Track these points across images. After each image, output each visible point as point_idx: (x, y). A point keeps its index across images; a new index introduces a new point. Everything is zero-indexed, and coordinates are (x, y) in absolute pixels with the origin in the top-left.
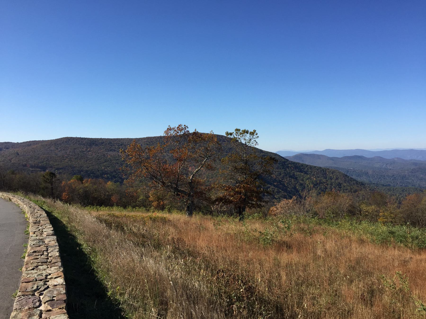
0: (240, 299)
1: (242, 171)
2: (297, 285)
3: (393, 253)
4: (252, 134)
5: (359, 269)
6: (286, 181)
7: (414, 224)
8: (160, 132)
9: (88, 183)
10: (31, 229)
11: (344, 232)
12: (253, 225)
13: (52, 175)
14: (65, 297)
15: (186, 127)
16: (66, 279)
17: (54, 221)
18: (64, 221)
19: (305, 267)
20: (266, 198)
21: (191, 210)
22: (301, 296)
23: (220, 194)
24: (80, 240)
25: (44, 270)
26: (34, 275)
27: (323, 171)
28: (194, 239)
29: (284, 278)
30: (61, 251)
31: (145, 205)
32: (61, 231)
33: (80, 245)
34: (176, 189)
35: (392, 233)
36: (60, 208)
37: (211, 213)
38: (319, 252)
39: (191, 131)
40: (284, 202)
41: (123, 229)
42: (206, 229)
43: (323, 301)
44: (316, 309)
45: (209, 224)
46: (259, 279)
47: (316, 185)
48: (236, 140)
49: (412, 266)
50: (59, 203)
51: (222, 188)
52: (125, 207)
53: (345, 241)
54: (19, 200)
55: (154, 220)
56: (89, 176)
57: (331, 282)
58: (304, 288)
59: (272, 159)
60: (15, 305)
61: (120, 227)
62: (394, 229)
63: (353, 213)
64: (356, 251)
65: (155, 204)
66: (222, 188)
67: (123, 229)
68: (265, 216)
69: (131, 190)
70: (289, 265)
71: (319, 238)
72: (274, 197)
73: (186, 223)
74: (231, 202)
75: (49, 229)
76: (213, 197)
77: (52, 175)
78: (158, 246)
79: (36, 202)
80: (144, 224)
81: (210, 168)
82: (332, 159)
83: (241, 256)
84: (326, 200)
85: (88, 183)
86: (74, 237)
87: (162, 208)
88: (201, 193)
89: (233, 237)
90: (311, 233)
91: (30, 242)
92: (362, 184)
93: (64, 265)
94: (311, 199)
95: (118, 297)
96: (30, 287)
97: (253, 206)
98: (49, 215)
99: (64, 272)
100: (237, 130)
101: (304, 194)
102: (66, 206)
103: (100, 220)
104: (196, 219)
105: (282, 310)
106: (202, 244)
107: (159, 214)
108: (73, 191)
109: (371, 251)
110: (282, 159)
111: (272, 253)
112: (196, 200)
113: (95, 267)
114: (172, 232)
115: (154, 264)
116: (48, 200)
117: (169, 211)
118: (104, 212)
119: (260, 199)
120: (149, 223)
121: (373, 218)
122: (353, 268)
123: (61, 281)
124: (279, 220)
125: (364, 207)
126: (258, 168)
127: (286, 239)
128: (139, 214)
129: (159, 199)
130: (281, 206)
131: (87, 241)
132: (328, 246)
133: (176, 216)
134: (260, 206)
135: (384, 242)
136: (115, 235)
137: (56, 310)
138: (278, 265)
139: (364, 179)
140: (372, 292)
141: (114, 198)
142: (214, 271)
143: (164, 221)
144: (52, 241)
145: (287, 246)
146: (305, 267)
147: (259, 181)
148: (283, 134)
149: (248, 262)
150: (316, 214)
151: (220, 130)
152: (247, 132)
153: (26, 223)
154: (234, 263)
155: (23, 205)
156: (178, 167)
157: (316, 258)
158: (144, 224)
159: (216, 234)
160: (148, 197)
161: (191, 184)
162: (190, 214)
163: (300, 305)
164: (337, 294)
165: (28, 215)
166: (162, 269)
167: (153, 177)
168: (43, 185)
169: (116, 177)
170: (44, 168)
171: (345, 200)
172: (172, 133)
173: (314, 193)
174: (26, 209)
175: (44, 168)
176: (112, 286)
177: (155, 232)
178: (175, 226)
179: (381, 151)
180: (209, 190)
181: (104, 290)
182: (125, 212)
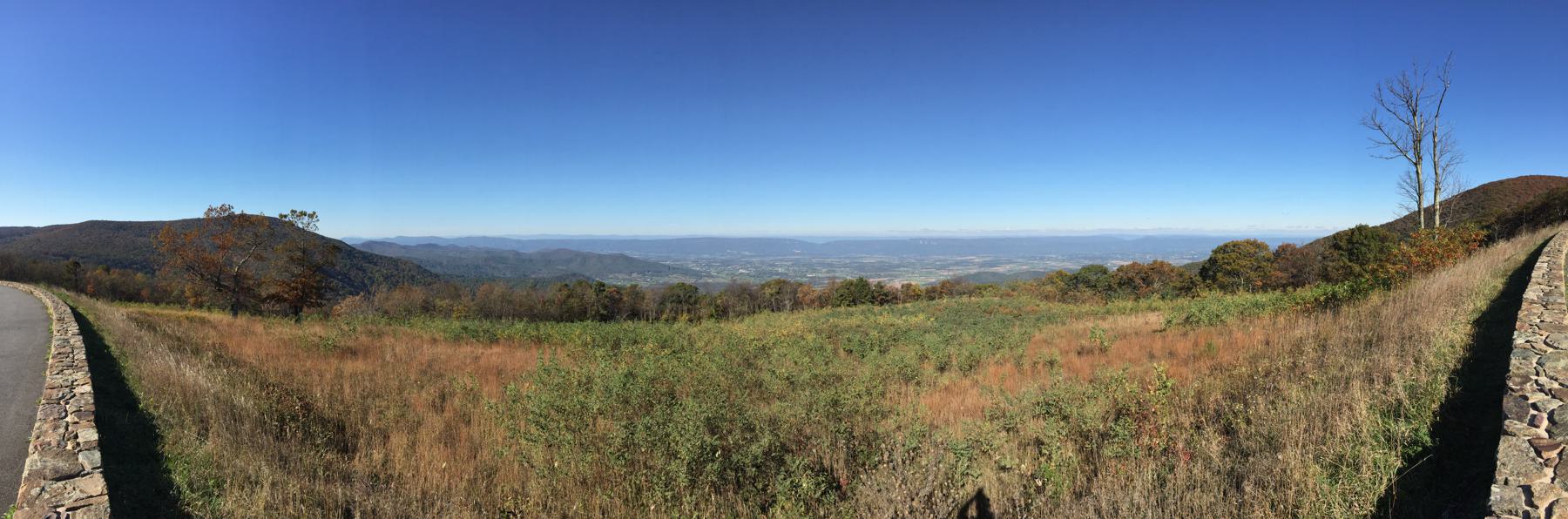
0: (293, 419)
1: (300, 262)
2: (363, 398)
3: (466, 350)
4: (311, 216)
5: (431, 372)
6: (353, 273)
7: (487, 316)
8: (198, 213)
9: (115, 275)
10: (55, 327)
11: (416, 331)
12: (312, 329)
13: (77, 264)
14: (93, 408)
15: (231, 207)
16: (94, 387)
17: (79, 318)
18: (91, 318)
19: (373, 375)
20: (328, 295)
21: (236, 309)
22: (365, 412)
23: (272, 291)
24: (109, 340)
25: (71, 376)
26: (59, 380)
27: (395, 262)
28: (239, 345)
29: (347, 390)
30: (88, 353)
31: (181, 301)
32: (88, 332)
33: (108, 347)
34: (218, 284)
35: (465, 328)
36: (85, 304)
37: (261, 313)
38: (388, 357)
39: (237, 212)
40: (349, 299)
41: (155, 329)
42: (253, 333)
43: (391, 414)
44: (382, 425)
45: (259, 327)
46: (319, 396)
47: (386, 278)
48: (292, 224)
49: (482, 362)
50: (84, 298)
51: (275, 282)
52: (157, 303)
53: (417, 342)
54: (40, 293)
55: (191, 320)
56: (116, 266)
57: (400, 391)
58: (369, 401)
59: (336, 247)
60: (39, 415)
61: (152, 328)
62: (466, 324)
63: (427, 309)
64: (428, 352)
65: (192, 300)
66: (275, 282)
67: (155, 329)
68: (327, 316)
69: (164, 283)
70: (353, 375)
71: (388, 341)
72: (338, 295)
73: (229, 325)
74: (285, 300)
75: (74, 328)
76: (264, 294)
77: (77, 264)
78: (197, 352)
79: (60, 296)
80: (180, 324)
81: (260, 258)
82: (405, 247)
83: (297, 365)
84: (397, 295)
85: (115, 275)
86: (102, 339)
87: (199, 306)
88: (249, 289)
89: (286, 343)
90: (380, 335)
91: (54, 343)
92: (437, 276)
93: (91, 370)
94: (380, 296)
95: (151, 410)
96: (55, 394)
97: (312, 305)
98: (74, 310)
99: (92, 378)
100: (293, 212)
101: (372, 289)
102: (93, 301)
103: (130, 318)
104: (242, 320)
105: (344, 429)
106: (248, 351)
107: (197, 313)
108: (98, 283)
109: (442, 350)
110: (1255, 327)
111: (334, 362)
112: (241, 297)
113: (124, 374)
114: (213, 337)
115: (193, 374)
116: (72, 294)
117: (209, 309)
118: (133, 308)
119: (321, 296)
120: (186, 324)
121: (447, 314)
122: (425, 373)
123: (88, 388)
124: (348, 320)
125: (438, 302)
126: (318, 258)
127: (351, 343)
128: (174, 312)
129: (196, 295)
130: (345, 305)
131: (116, 343)
132: (397, 350)
133: (216, 316)
134: (320, 305)
135: (457, 339)
136: (147, 337)
137: (83, 422)
138: (339, 375)
139: (437, 270)
140: (443, 397)
141: (144, 293)
142: (264, 385)
143: (203, 321)
144: (77, 341)
145: (353, 353)
146: (373, 375)
147: (320, 275)
148: (351, 216)
149: (305, 374)
150: (386, 312)
151: (273, 213)
152: (304, 214)
153: (49, 319)
154: (289, 375)
155: (48, 300)
156: (219, 257)
157: (384, 364)
158: (180, 324)
159: (264, 338)
160: (183, 292)
161: (237, 278)
162: (235, 314)
163: (364, 421)
164: (406, 405)
165: (51, 311)
166: (202, 381)
167: (190, 268)
168: (67, 276)
169: (147, 267)
170: (67, 257)
171: (418, 294)
172: (214, 214)
173: (384, 288)
174: (49, 303)
175: (67, 257)
176: (146, 399)
177: (192, 334)
178: (215, 328)
179: (930, 240)
180: (259, 285)
181: (136, 401)
182: (157, 310)
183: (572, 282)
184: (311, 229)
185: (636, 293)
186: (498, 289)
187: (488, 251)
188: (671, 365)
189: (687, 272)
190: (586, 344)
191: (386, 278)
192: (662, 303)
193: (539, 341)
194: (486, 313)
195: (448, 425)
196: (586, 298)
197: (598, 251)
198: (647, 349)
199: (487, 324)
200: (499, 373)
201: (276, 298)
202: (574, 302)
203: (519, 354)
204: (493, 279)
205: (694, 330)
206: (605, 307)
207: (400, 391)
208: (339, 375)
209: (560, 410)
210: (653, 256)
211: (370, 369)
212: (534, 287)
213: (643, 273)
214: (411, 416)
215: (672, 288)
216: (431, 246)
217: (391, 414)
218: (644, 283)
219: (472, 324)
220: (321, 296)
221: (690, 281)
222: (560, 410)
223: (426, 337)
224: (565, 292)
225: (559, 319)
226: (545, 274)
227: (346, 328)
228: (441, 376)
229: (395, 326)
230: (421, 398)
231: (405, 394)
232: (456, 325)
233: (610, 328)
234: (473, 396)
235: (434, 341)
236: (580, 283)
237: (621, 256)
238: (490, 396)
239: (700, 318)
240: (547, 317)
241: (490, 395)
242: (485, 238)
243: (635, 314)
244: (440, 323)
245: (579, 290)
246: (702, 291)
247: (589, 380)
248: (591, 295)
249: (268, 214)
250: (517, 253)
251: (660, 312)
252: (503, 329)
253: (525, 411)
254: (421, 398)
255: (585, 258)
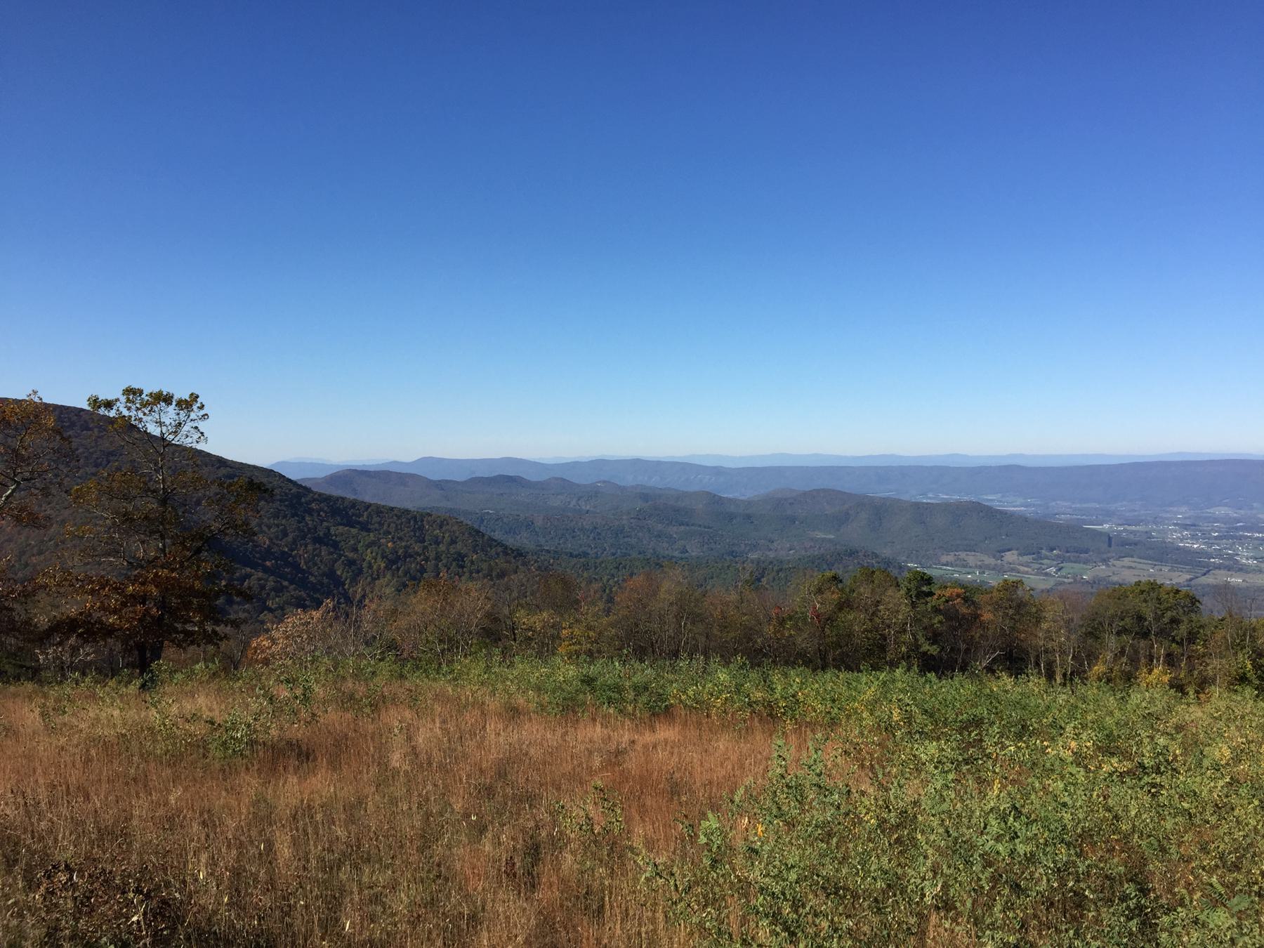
1: (153, 526)
3: (591, 733)
4: (186, 405)
5: (504, 790)
6: (303, 554)
7: (641, 653)
12: (191, 701)
19: (353, 809)
22: (334, 904)
27: (415, 521)
29: (284, 851)
35: (588, 681)
37: (34, 673)
38: (396, 759)
40: (294, 620)
43: (400, 903)
47: (393, 561)
48: (128, 427)
49: (632, 764)
53: (470, 717)
57: (426, 840)
59: (255, 485)
62: (593, 670)
63: (495, 635)
64: (498, 738)
68: (230, 666)
71: (394, 718)
74: (109, 631)
76: (42, 620)
82: (440, 485)
84: (421, 604)
90: (376, 706)
92: (519, 554)
97: (190, 639)
109: (536, 735)
111: (250, 784)
121: (544, 646)
122: (489, 792)
125: (523, 618)
126: (208, 517)
127: (297, 731)
130: (285, 634)
132: (420, 740)
134: (213, 638)
135: (569, 708)
138: (263, 817)
139: (522, 540)
140: (534, 851)
146: (353, 809)
150: (392, 646)
151: (71, 393)
152: (168, 399)
164: (441, 875)
171: (473, 599)
173: (387, 586)
180: (27, 595)
183: (849, 571)
184: (187, 439)
185: (1016, 604)
186: (670, 587)
187: (645, 495)
188: (1133, 804)
189: (1163, 553)
190: (890, 729)
191: (393, 561)
192: (1093, 633)
193: (770, 715)
194: (641, 644)
195: (546, 923)
196: (900, 606)
197: (912, 494)
198: (1069, 756)
199: (644, 672)
200: (675, 790)
201: (84, 628)
202: (856, 621)
203: (722, 743)
204: (658, 563)
205: (1193, 713)
206: (935, 638)
207: (426, 840)
208: (263, 817)
209: (834, 890)
210: (1064, 510)
211: (348, 792)
212: (755, 581)
213: (1036, 553)
214: (453, 902)
215: (1120, 593)
216: (505, 481)
217: (400, 903)
218: (1039, 578)
219: (610, 671)
220: (215, 615)
221: (1172, 577)
222: (834, 890)
223: (493, 704)
224: (833, 596)
225: (818, 661)
226: (784, 549)
227: (284, 693)
228: (531, 799)
229: (415, 680)
230: (477, 858)
231: (438, 850)
232: (568, 672)
233: (955, 691)
234: (611, 849)
235: (513, 713)
236: (870, 575)
237: (971, 507)
238: (650, 844)
239: (1203, 684)
240: (789, 657)
241: (650, 854)
242: (637, 464)
243: (1014, 660)
244: (525, 669)
245: (865, 591)
246: (1211, 609)
247: (907, 819)
248: (896, 605)
249: (52, 396)
250: (715, 500)
251: (1085, 657)
252: (680, 683)
253: (744, 887)
254: (477, 858)
255: (880, 512)
